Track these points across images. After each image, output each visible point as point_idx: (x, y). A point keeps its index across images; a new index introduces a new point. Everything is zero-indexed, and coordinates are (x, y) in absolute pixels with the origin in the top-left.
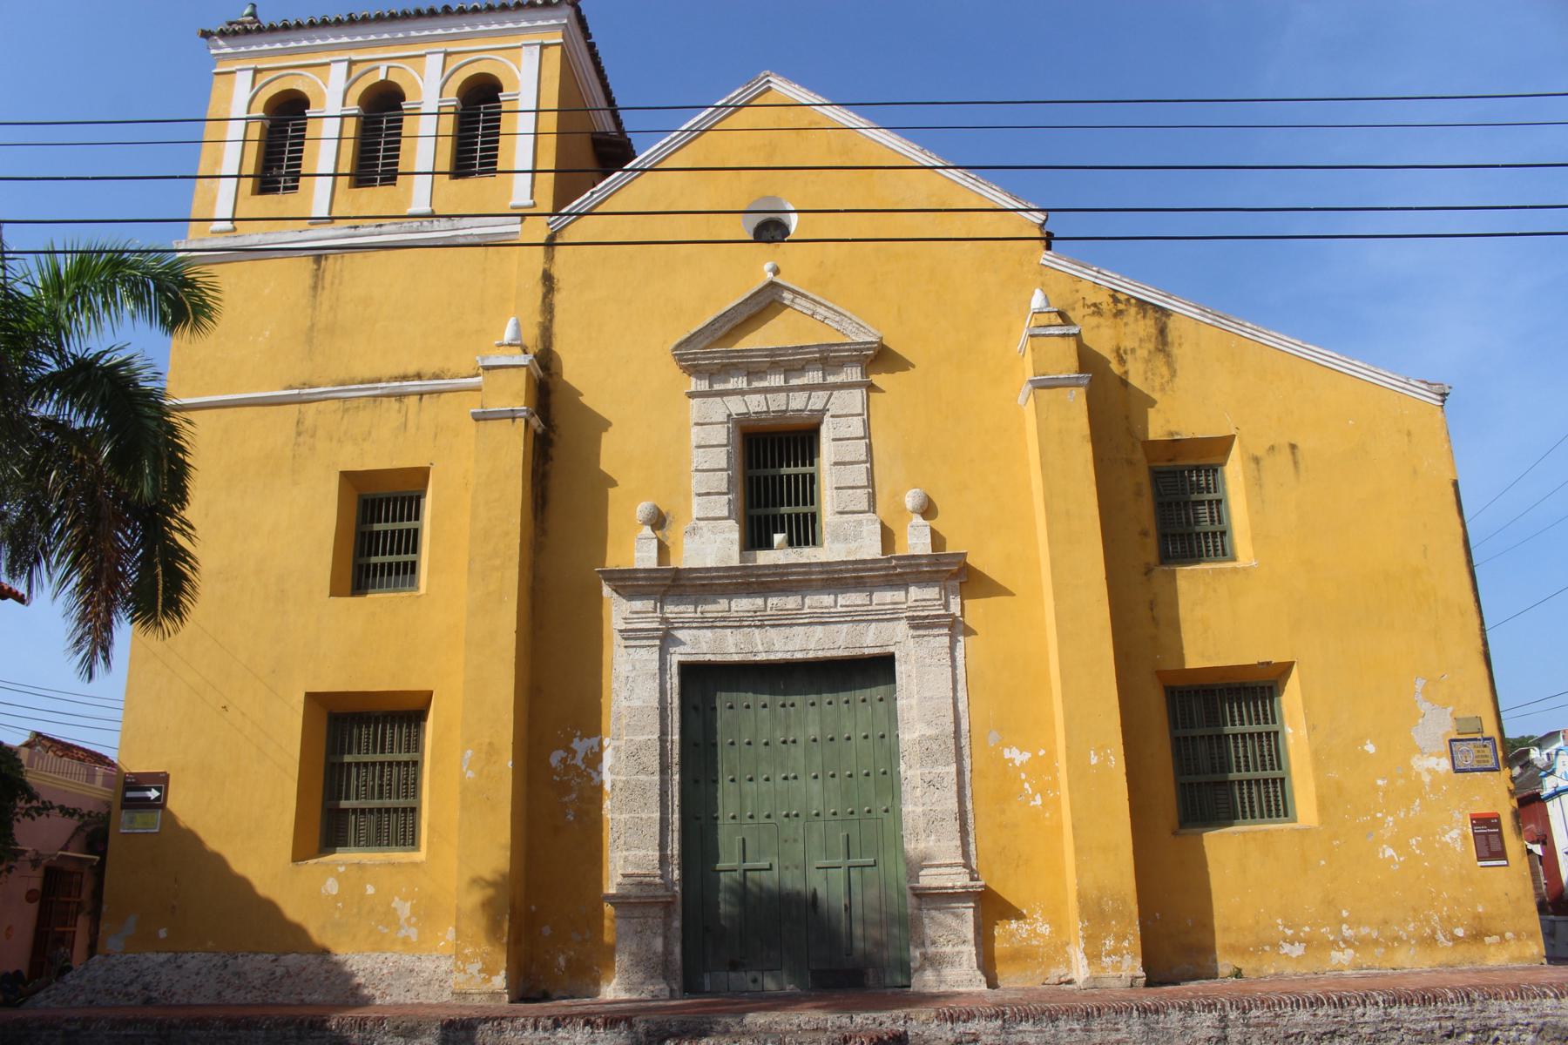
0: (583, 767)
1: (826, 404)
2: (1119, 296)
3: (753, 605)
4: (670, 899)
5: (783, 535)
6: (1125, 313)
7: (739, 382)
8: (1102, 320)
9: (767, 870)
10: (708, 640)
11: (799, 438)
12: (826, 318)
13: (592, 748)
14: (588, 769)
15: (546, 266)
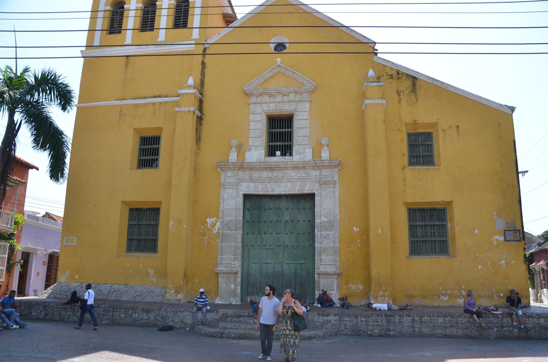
0: (210, 228)
1: (296, 108)
4: (236, 272)
6: (401, 78)
7: (266, 99)
8: (393, 80)
10: (252, 187)
12: (297, 78)
13: (213, 221)
14: (212, 229)
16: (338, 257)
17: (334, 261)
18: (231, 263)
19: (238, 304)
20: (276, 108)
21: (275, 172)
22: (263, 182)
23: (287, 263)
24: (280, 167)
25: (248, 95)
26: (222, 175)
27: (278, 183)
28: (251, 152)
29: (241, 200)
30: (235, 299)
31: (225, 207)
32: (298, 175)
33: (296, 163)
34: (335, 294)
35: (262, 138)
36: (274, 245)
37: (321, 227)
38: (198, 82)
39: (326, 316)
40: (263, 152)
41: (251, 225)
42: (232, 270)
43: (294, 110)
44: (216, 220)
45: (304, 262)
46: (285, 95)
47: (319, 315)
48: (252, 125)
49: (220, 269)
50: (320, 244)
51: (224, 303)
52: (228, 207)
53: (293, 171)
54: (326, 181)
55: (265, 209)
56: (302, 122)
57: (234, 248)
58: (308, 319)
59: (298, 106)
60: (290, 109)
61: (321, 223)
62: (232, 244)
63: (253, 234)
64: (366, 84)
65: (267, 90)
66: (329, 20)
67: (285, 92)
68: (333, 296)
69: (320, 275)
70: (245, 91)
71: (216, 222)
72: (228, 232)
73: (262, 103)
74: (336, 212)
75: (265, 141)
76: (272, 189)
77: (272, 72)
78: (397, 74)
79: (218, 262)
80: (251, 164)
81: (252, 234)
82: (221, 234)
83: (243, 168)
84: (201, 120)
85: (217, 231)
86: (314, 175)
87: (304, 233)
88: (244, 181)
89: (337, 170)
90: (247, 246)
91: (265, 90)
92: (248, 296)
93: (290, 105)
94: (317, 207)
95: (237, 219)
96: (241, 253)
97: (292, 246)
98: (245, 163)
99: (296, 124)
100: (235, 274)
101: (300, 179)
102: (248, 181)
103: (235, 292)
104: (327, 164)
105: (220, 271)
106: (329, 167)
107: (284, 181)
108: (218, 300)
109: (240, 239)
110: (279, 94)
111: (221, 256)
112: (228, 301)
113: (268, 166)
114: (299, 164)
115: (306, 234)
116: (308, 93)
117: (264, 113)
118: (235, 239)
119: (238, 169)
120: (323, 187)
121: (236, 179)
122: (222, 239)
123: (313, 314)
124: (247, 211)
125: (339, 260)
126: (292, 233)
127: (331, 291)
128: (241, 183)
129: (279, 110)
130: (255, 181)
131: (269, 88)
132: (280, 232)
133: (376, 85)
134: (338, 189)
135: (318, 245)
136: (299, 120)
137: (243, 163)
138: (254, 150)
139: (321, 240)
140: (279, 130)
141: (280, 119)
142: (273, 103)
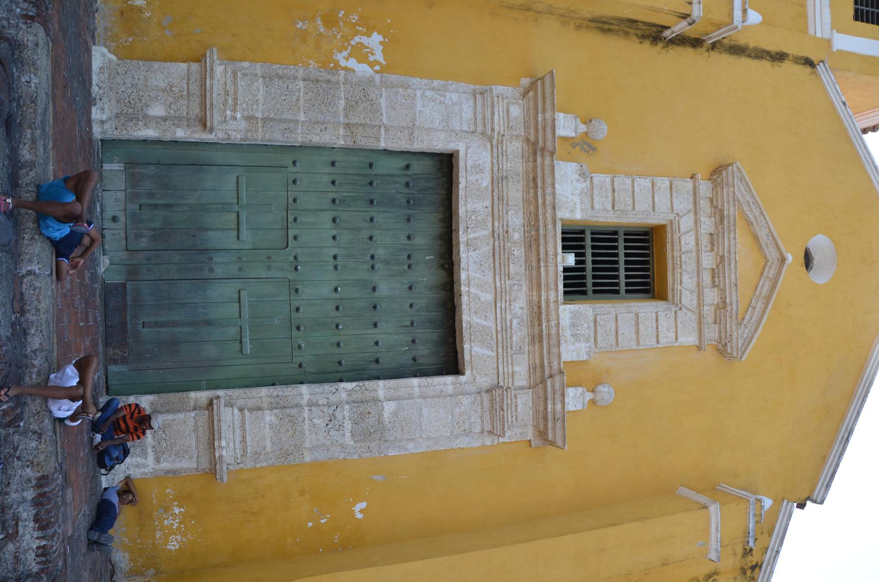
0: (352, 43)
1: (685, 307)
2: (757, 570)
3: (513, 230)
4: (208, 124)
5: (574, 264)
6: (744, 577)
7: (707, 224)
8: (739, 557)
10: (480, 181)
11: (648, 280)
12: (754, 308)
13: (373, 54)
14: (350, 48)
15: (791, 56)
16: (271, 462)
17: (256, 453)
18: (238, 107)
19: (94, 130)
20: (684, 253)
21: (523, 250)
22: (493, 214)
23: (242, 293)
24: (539, 267)
25: (717, 172)
26: (510, 89)
27: (491, 260)
28: (578, 180)
29: (440, 144)
30: (110, 118)
31: (419, 93)
32: (515, 322)
33: (553, 316)
34: (145, 466)
35: (612, 212)
36: (299, 251)
37: (362, 402)
38: (742, 41)
39: (36, 515)
40: (578, 216)
41: (358, 175)
42: (215, 110)
43: (680, 302)
44: (377, 62)
45: (248, 348)
46: (713, 277)
47: (39, 486)
48: (643, 183)
49: (219, 70)
50: (311, 404)
51: (95, 78)
52: (419, 103)
53: (525, 306)
54: (503, 410)
55: (408, 220)
56: (652, 328)
57: (290, 117)
58: (16, 438)
59: (689, 314)
60: (683, 291)
61: (376, 400)
62: (302, 114)
63: (333, 183)
64: (751, 500)
65: (732, 228)
66: (865, 383)
67: (725, 277)
68: (139, 459)
69: (207, 409)
70: (730, 168)
71: (372, 64)
72: (339, 99)
73: (696, 214)
74: (411, 446)
75: (601, 220)
76: (474, 241)
77: (769, 243)
78: (752, 566)
79: (239, 64)
80: (549, 180)
81: (330, 180)
82: (334, 79)
83: (535, 154)
84: (651, 39)
85: (343, 63)
86: (516, 369)
87: (338, 345)
88: (495, 155)
89: (530, 436)
90: (294, 163)
91: (732, 223)
92: (126, 164)
93: (692, 292)
94: (423, 384)
95: (383, 130)
96: (275, 141)
97: (297, 309)
98: (553, 161)
99: (646, 308)
100: (201, 120)
101: (505, 329)
102: (495, 169)
103: (138, 119)
104: (549, 410)
105: (212, 69)
106: (541, 416)
107: (498, 280)
108: (104, 55)
109: (318, 138)
110: (719, 261)
111: (260, 74)
112: (101, 91)
113: (541, 231)
114: (548, 327)
115: (337, 351)
116: (721, 339)
117: (672, 218)
118: (318, 122)
119: (532, 138)
120: (482, 402)
121: (502, 132)
122: (317, 81)
123: (42, 458)
124: (402, 163)
125: (261, 468)
126: (337, 308)
127: (155, 451)
128: (489, 145)
129: (681, 261)
130: (496, 190)
131: (735, 233)
132: (339, 267)
133: (748, 527)
134: (476, 444)
135: (306, 397)
136: (657, 316)
137: (552, 153)
138: (583, 188)
139: (324, 405)
140: (622, 259)
141: (646, 262)
142: (697, 244)
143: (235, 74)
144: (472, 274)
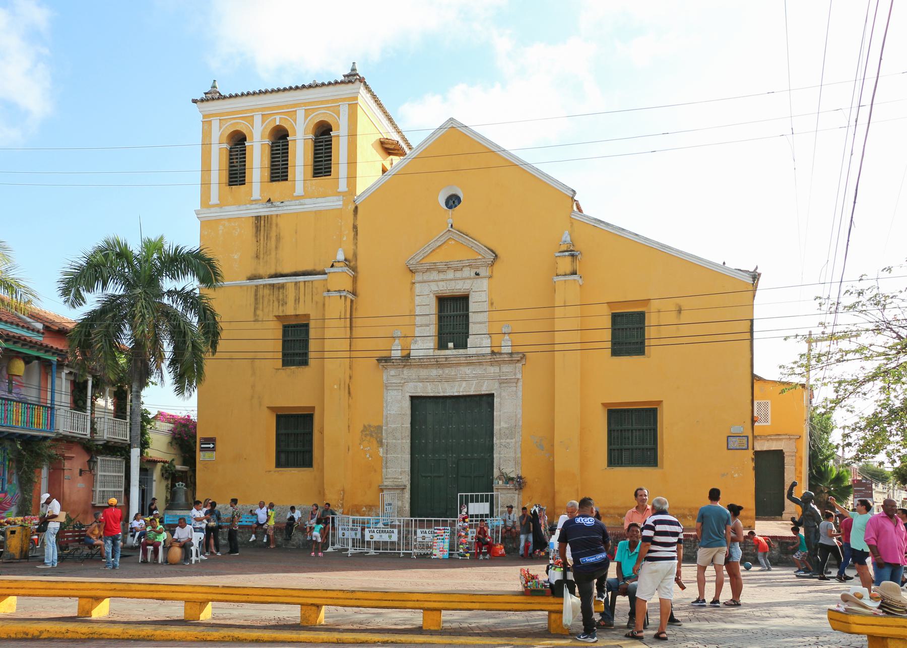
7: (434, 275)
9: (728, 446)
32: (474, 373)
50: (499, 454)
52: (392, 412)
59: (474, 284)
61: (500, 430)
120: (504, 387)
135: (498, 455)
143: (386, 478)
144: (455, 391)
